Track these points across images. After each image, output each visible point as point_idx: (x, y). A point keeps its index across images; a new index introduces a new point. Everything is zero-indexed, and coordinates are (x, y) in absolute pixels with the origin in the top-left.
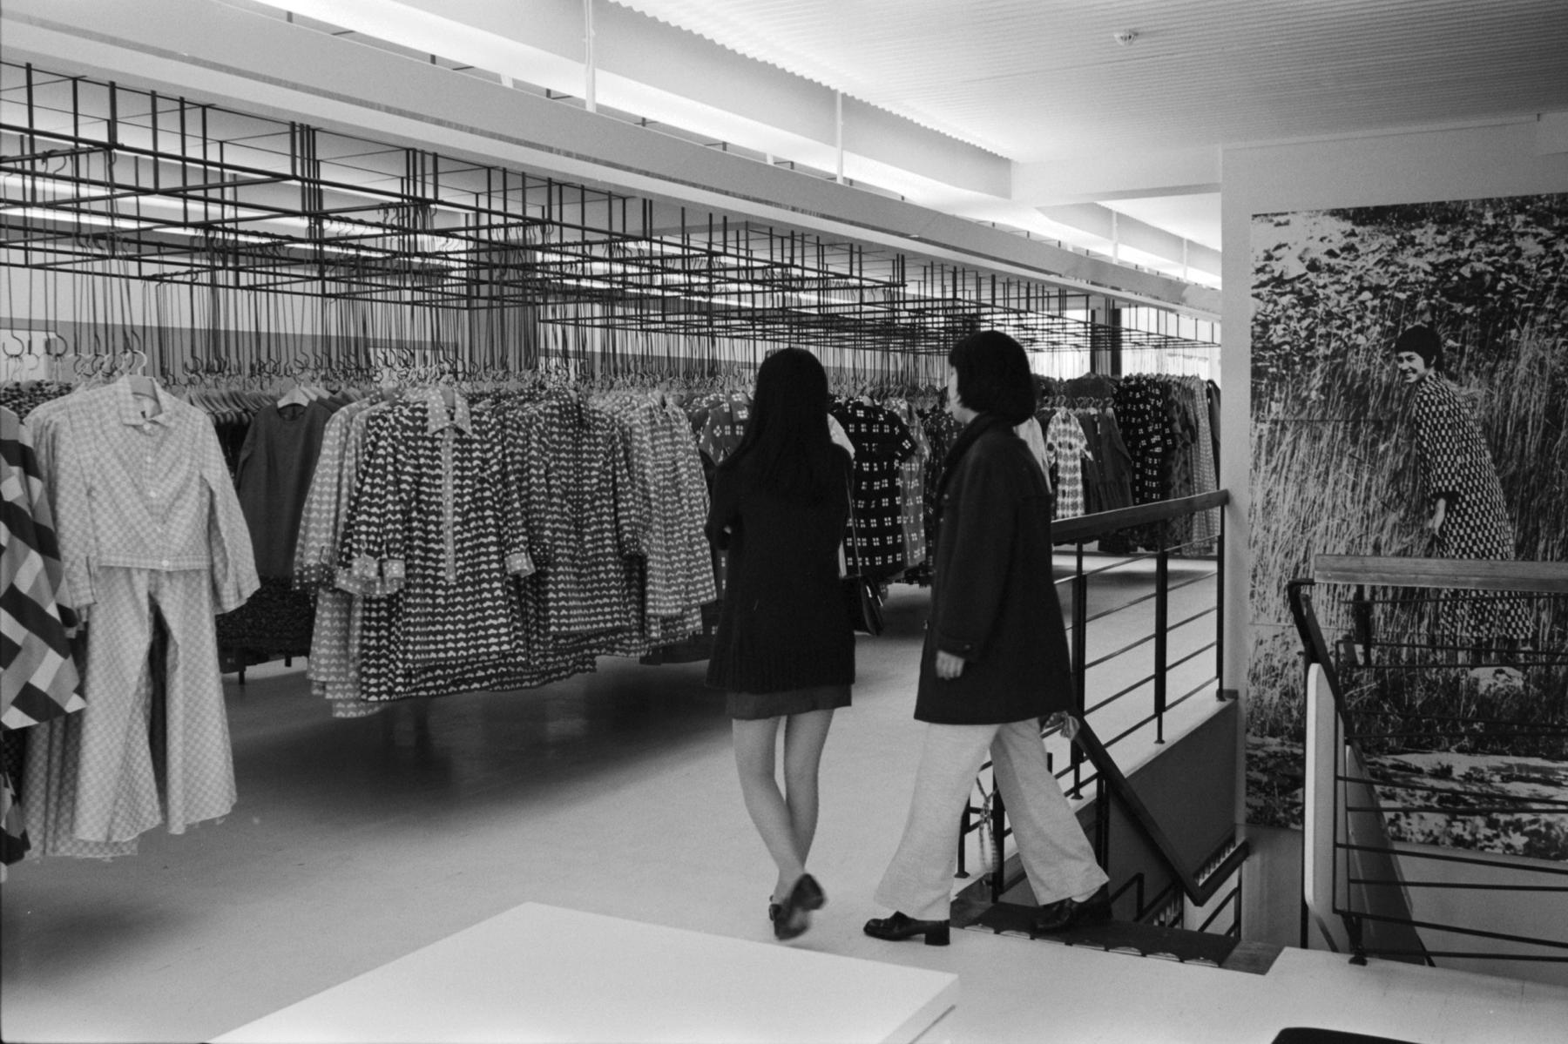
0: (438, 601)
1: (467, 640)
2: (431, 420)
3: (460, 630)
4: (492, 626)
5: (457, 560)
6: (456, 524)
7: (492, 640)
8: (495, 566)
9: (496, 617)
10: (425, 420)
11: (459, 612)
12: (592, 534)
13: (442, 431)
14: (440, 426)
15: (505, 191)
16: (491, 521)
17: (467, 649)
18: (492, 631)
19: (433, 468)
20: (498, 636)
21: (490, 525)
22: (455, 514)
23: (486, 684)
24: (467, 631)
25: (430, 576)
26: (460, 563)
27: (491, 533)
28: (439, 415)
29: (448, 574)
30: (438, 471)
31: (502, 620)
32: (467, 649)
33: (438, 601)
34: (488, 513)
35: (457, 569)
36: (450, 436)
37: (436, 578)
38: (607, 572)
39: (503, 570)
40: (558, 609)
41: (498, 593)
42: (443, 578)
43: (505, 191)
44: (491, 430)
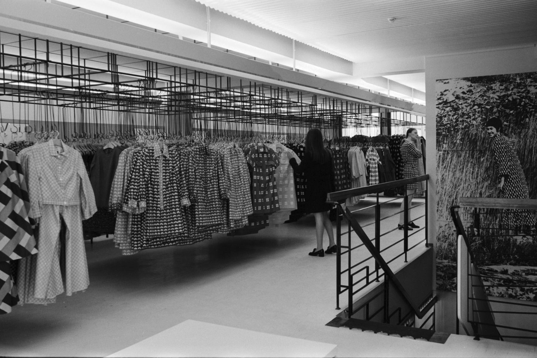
0: (158, 215)
1: (167, 228)
2: (155, 153)
3: (165, 225)
4: (176, 224)
5: (164, 201)
6: (163, 189)
7: (176, 228)
8: (177, 203)
9: (177, 221)
10: (153, 153)
11: (165, 219)
12: (210, 191)
13: (159, 157)
14: (158, 155)
15: (180, 75)
16: (176, 187)
17: (167, 231)
18: (176, 225)
19: (156, 169)
20: (178, 227)
21: (175, 189)
22: (164, 185)
23: (174, 243)
24: (167, 225)
25: (155, 206)
26: (165, 202)
27: (176, 192)
28: (159, 152)
29: (161, 206)
30: (157, 171)
31: (180, 221)
32: (167, 231)
33: (158, 215)
34: (175, 185)
35: (164, 204)
36: (162, 159)
37: (157, 207)
38: (216, 205)
39: (180, 204)
40: (199, 217)
41: (178, 212)
42: (159, 207)
43: (180, 75)
44: (175, 156)
